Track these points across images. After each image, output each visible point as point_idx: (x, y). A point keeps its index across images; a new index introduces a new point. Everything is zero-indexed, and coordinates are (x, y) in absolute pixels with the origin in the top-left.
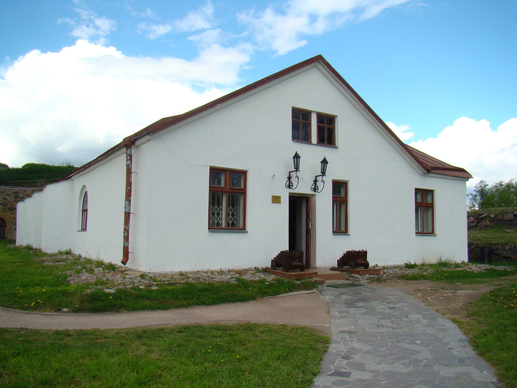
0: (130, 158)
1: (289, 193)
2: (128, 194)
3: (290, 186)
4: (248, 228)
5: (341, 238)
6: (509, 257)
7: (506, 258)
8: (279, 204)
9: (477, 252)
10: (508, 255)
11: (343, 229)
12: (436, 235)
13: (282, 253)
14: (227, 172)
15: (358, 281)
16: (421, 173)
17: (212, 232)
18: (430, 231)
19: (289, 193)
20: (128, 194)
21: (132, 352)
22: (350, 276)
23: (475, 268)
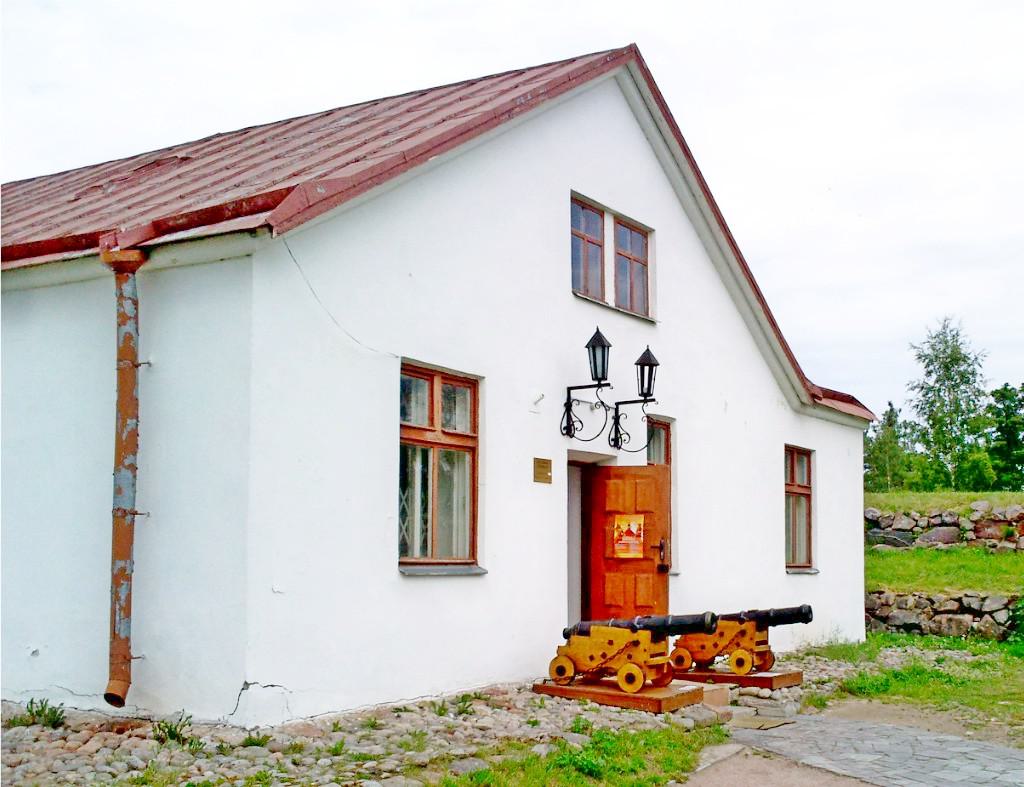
0: (128, 319)
1: (570, 452)
2: (127, 446)
3: (569, 430)
4: (484, 559)
5: (444, 593)
6: (917, 627)
7: (909, 628)
8: (546, 485)
9: (875, 615)
10: (913, 620)
11: (801, 559)
12: (481, 574)
13: (774, 625)
14: (437, 381)
15: (777, 706)
16: (796, 403)
17: (411, 576)
18: (461, 552)
19: (570, 452)
20: (127, 446)
21: (987, 731)
22: (741, 695)
23: (894, 656)
